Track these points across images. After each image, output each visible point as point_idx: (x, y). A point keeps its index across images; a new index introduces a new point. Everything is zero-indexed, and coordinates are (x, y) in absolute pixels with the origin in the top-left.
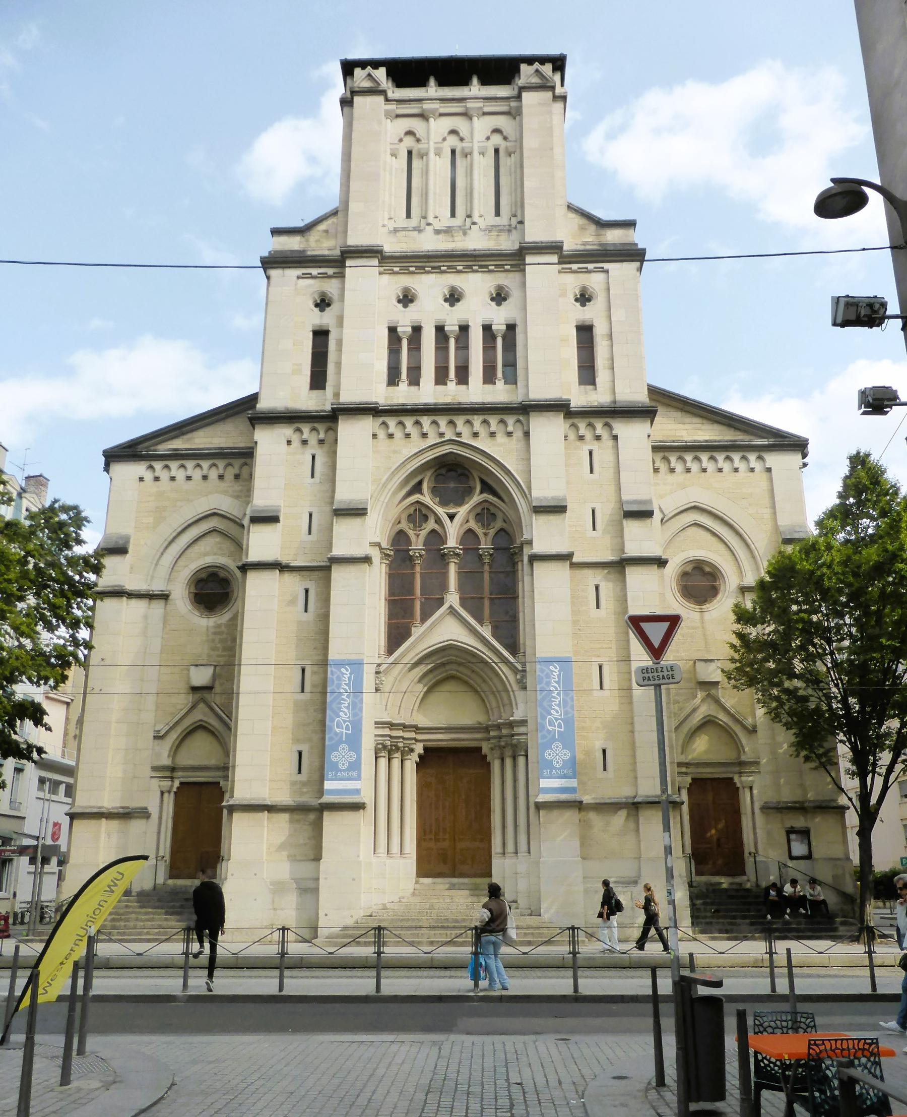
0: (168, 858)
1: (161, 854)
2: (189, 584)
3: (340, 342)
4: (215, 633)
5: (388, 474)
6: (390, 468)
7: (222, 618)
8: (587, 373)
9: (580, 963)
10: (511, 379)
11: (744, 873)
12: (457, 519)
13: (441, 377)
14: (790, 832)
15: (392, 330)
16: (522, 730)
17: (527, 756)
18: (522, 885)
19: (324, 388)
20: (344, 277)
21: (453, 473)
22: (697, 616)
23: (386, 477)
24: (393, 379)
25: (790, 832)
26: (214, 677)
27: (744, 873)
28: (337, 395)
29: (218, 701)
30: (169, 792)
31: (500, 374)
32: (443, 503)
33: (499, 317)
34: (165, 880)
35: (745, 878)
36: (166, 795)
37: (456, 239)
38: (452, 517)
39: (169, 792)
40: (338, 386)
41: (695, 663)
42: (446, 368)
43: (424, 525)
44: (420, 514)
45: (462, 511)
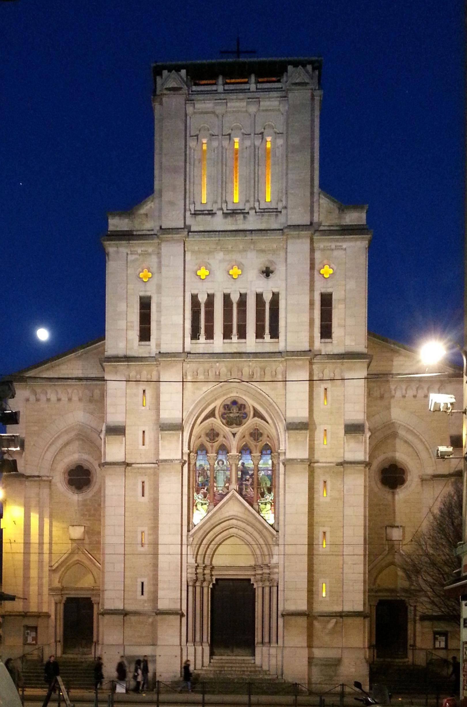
0: (62, 640)
1: (58, 639)
2: (64, 473)
3: (159, 305)
4: (83, 505)
5: (193, 405)
6: (195, 401)
7: (89, 493)
8: (145, 335)
9: (303, 621)
10: (275, 334)
11: (407, 657)
12: (237, 436)
13: (227, 335)
14: (436, 633)
15: (194, 298)
16: (276, 570)
17: (278, 587)
18: (273, 661)
19: (149, 340)
20: (308, 658)
21: (234, 412)
22: (390, 497)
23: (192, 407)
24: (195, 335)
25: (436, 633)
26: (86, 532)
27: (407, 657)
28: (158, 345)
29: (87, 548)
30: (60, 603)
31: (267, 331)
32: (229, 423)
33: (267, 288)
34: (62, 654)
35: (407, 660)
36: (59, 605)
37: (239, 222)
38: (234, 435)
39: (60, 603)
40: (159, 339)
41: (386, 527)
42: (231, 327)
43: (217, 439)
44: (213, 435)
45: (240, 430)
